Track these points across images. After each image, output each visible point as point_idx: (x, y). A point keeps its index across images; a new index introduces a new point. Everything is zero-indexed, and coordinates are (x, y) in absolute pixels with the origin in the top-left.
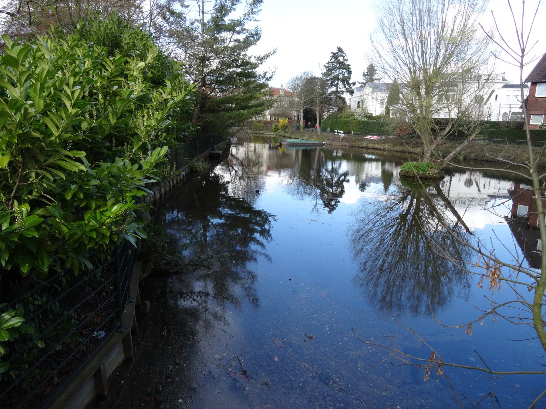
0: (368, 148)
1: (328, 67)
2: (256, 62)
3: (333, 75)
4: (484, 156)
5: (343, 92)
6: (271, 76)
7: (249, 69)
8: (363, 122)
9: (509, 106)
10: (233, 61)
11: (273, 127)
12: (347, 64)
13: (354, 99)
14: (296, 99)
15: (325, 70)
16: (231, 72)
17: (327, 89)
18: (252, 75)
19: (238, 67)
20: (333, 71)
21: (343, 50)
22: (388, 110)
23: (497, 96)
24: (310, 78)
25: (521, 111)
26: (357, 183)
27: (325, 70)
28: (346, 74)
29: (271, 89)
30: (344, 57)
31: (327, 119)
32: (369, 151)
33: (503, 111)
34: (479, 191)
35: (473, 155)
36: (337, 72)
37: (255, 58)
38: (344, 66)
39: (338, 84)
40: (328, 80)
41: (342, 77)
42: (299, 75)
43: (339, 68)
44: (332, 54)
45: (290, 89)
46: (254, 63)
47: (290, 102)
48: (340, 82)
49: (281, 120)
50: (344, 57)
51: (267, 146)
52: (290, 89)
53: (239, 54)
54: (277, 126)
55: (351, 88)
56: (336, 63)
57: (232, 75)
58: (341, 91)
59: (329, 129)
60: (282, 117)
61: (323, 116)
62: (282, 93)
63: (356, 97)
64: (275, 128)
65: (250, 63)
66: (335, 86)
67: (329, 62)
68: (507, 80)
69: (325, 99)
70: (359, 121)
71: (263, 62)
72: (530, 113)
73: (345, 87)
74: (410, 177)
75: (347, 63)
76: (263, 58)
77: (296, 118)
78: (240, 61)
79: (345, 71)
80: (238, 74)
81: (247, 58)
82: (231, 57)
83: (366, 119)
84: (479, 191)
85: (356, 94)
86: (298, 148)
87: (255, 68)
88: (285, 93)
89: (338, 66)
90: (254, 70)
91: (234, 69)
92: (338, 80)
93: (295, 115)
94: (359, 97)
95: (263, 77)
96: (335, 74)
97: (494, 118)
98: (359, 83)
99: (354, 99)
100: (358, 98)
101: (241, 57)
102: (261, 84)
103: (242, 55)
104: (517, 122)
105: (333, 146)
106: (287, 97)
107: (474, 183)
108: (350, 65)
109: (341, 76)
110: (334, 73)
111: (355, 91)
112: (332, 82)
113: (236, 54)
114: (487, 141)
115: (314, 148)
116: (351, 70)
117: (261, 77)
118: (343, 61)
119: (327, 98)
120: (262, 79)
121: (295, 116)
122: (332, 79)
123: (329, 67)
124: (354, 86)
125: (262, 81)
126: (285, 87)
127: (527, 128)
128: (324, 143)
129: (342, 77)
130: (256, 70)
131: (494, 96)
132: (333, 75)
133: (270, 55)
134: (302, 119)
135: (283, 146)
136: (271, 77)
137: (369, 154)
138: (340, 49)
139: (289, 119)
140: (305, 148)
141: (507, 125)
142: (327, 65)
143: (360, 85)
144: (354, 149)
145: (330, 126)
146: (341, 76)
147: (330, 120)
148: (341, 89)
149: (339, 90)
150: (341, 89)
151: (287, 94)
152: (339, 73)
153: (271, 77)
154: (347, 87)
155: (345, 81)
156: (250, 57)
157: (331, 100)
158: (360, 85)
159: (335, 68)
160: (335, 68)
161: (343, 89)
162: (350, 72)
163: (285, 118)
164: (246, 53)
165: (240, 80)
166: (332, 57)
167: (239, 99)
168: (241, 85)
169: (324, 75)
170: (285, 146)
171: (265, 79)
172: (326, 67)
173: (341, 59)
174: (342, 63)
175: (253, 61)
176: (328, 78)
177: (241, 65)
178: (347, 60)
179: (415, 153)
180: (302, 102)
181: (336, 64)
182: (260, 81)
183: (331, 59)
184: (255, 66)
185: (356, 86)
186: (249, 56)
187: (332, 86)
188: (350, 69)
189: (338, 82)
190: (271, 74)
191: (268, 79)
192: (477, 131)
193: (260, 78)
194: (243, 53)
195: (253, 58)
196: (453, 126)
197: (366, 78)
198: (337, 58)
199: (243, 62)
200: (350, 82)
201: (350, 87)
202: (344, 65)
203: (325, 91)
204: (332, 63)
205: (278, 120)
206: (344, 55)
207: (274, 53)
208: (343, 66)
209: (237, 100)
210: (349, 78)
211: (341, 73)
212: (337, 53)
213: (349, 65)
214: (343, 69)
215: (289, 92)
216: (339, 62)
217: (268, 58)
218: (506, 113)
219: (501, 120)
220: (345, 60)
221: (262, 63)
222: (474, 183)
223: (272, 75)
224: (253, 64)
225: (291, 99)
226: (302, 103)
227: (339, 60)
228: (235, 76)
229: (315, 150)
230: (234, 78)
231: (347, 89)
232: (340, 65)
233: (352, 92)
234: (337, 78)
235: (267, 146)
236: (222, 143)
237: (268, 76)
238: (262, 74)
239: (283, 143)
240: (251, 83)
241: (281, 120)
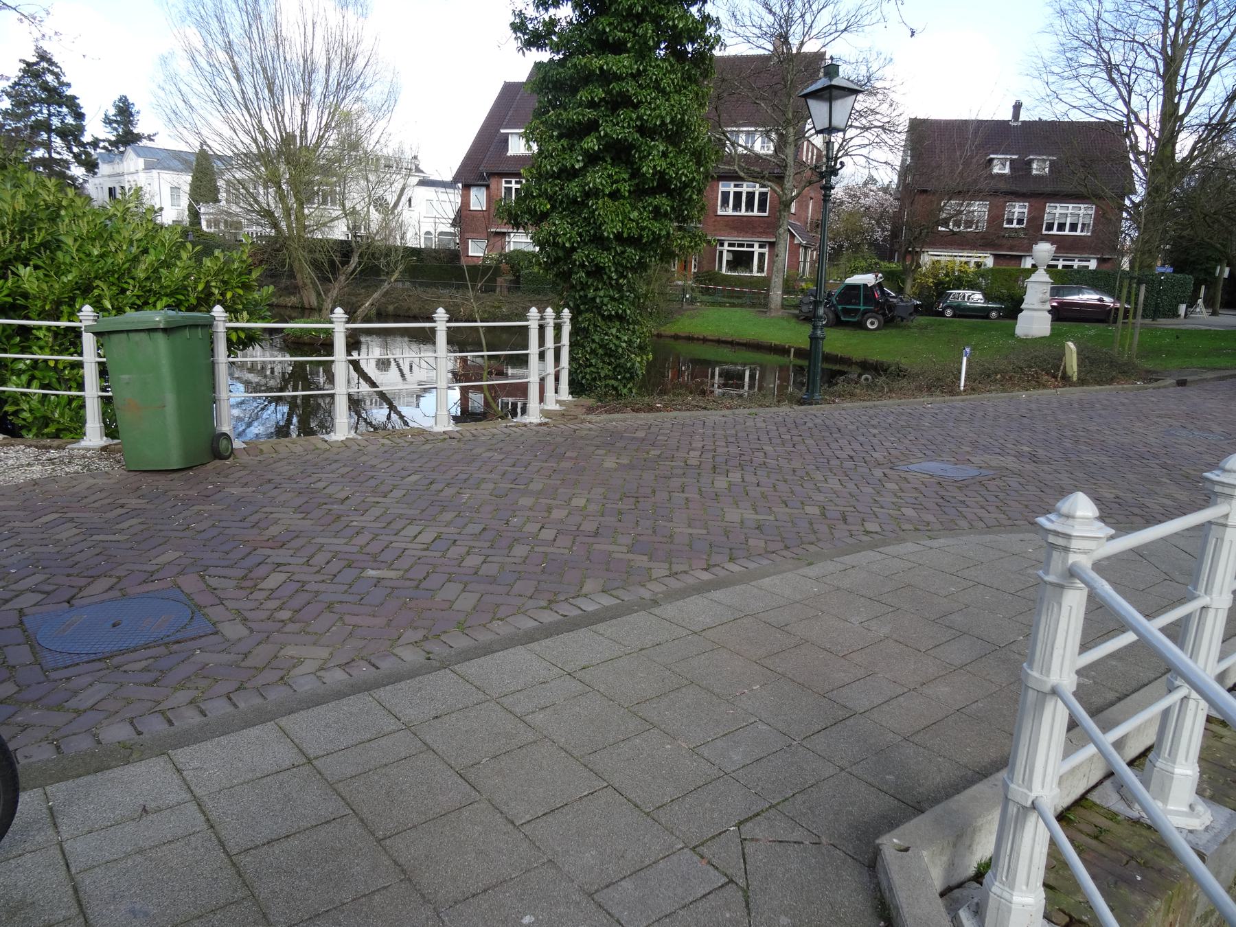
4: (409, 309)
5: (66, 162)
9: (432, 220)
12: (68, 93)
21: (55, 59)
22: (195, 215)
23: (410, 200)
25: (878, 841)
28: (70, 120)
30: (57, 76)
33: (423, 230)
34: (403, 375)
35: (391, 308)
38: (57, 96)
44: (23, 66)
50: (57, 76)
68: (422, 172)
72: (467, 235)
73: (70, 150)
74: (305, 344)
75: (69, 92)
84: (403, 375)
85: (104, 169)
92: (50, 130)
94: (110, 176)
96: (40, 117)
97: (412, 242)
100: (107, 179)
104: (449, 250)
107: (393, 364)
108: (77, 98)
110: (35, 114)
114: (408, 284)
116: (82, 111)
127: (463, 262)
131: (404, 199)
132: (33, 118)
138: (43, 56)
141: (434, 254)
146: (55, 122)
152: (50, 115)
155: (71, 135)
159: (35, 100)
160: (35, 100)
162: (80, 116)
166: (25, 71)
174: (55, 89)
178: (69, 85)
179: (285, 307)
188: (78, 106)
192: (400, 268)
196: (361, 256)
197: (115, 129)
200: (86, 138)
202: (60, 95)
204: (25, 86)
206: (56, 70)
210: (81, 129)
212: (37, 63)
214: (60, 106)
216: (45, 87)
218: (428, 233)
219: (423, 246)
220: (62, 84)
222: (393, 364)
234: (46, 126)
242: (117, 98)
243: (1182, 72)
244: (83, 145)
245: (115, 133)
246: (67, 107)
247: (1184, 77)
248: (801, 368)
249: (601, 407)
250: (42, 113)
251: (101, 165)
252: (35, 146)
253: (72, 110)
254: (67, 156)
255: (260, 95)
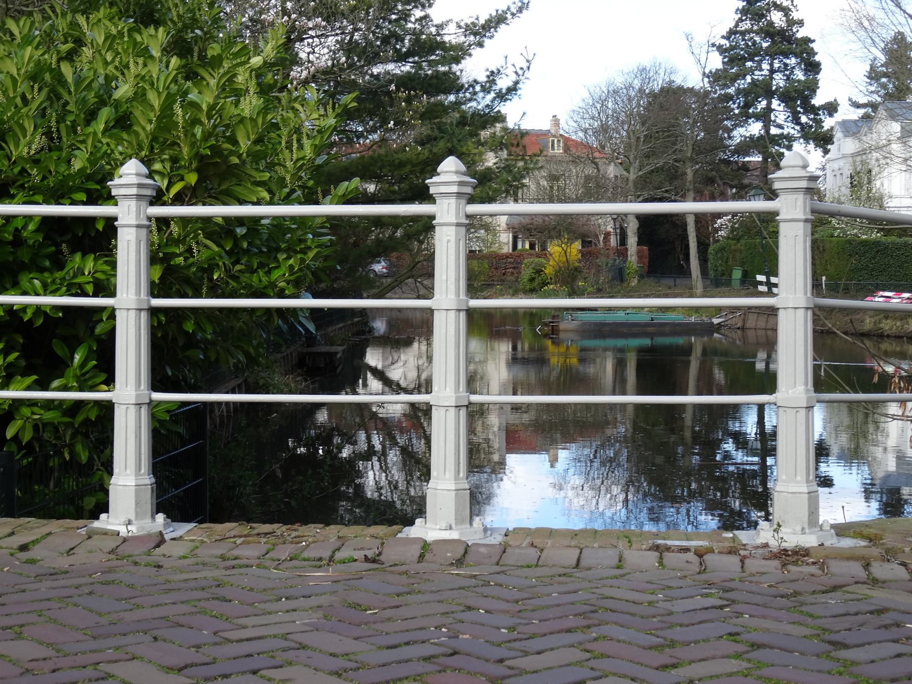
0: (881, 336)
1: (726, 50)
2: (462, 39)
3: (749, 79)
5: (790, 138)
6: (510, 84)
7: (437, 63)
8: (865, 243)
10: (386, 40)
11: (526, 273)
13: (835, 165)
14: (612, 171)
15: (716, 62)
16: (377, 77)
17: (729, 131)
18: (450, 83)
19: (401, 58)
20: (749, 64)
24: (662, 89)
26: (867, 498)
27: (716, 62)
28: (799, 75)
29: (502, 463)
31: (728, 238)
32: (886, 346)
36: (765, 66)
37: (460, 27)
39: (769, 110)
40: (728, 98)
41: (782, 84)
42: (619, 81)
43: (772, 54)
45: (585, 131)
46: (453, 42)
47: (588, 178)
48: (775, 103)
49: (554, 248)
51: (504, 347)
52: (585, 131)
53: (405, 16)
54: (539, 272)
55: (819, 122)
56: (757, 33)
57: (383, 86)
58: (782, 136)
59: (737, 274)
60: (559, 237)
61: (716, 230)
62: (559, 151)
63: (844, 156)
64: (532, 280)
65: (442, 45)
66: (758, 117)
67: (732, 33)
69: (722, 166)
70: (849, 242)
71: (487, 42)
73: (796, 120)
76: (483, 27)
77: (613, 241)
78: (408, 37)
79: (792, 61)
80: (405, 82)
81: (433, 30)
82: (378, 26)
83: (875, 236)
85: (844, 145)
86: (620, 343)
87: (457, 61)
88: (567, 149)
89: (765, 45)
90: (455, 68)
91: (390, 67)
92: (769, 94)
93: (610, 228)
95: (486, 90)
98: (857, 105)
99: (835, 165)
101: (410, 25)
102: (476, 114)
103: (413, 19)
105: (751, 334)
106: (575, 161)
109: (779, 80)
110: (751, 71)
111: (838, 135)
112: (747, 105)
113: (394, 17)
115: (680, 341)
116: (817, 58)
117: (478, 88)
118: (784, 25)
119: (727, 162)
120: (481, 95)
121: (607, 234)
122: (745, 92)
123: (732, 48)
124: (831, 115)
125: (483, 101)
126: (569, 127)
128: (716, 321)
129: (782, 84)
130: (460, 66)
132: (749, 79)
133: (509, 16)
134: (632, 240)
135: (562, 335)
136: (513, 89)
137: (887, 356)
139: (585, 243)
140: (646, 342)
142: (724, 42)
143: (861, 112)
144: (829, 341)
145: (742, 264)
146: (779, 80)
147: (743, 242)
148: (780, 127)
149: (774, 131)
150: (780, 127)
151: (574, 150)
152: (772, 71)
153: (513, 89)
154: (804, 119)
156: (440, 27)
157: (747, 170)
158: (861, 112)
160: (754, 53)
161: (791, 129)
162: (813, 67)
163: (571, 241)
164: (429, 11)
165: (409, 100)
167: (408, 162)
168: (412, 118)
169: (716, 77)
170: (572, 336)
171: (493, 95)
172: (720, 49)
173: (777, 18)
175: (451, 36)
176: (731, 91)
177: (410, 53)
178: (801, 23)
180: (632, 176)
181: (757, 39)
182: (474, 104)
183: (741, 20)
184: (458, 53)
185: (839, 117)
186: (437, 20)
187: (749, 117)
188: (813, 53)
189: (769, 103)
190: (514, 77)
191: (502, 96)
193: (475, 93)
194: (418, 13)
195: (451, 28)
197: (884, 86)
198: (763, 16)
199: (416, 41)
201: (814, 120)
203: (722, 139)
204: (743, 33)
205: (544, 248)
207: (520, 10)
208: (785, 46)
209: (402, 164)
210: (812, 87)
211: (779, 71)
213: (807, 41)
215: (578, 144)
216: (769, 32)
217: (503, 26)
220: (791, 22)
221: (480, 45)
223: (517, 83)
224: (453, 47)
225: (590, 170)
226: (631, 184)
227: (771, 24)
228: (393, 87)
229: (687, 351)
230: (389, 93)
231: (803, 127)
232: (773, 42)
233: (824, 140)
234: (764, 89)
235: (504, 347)
236: (341, 325)
237: (503, 83)
238: (482, 78)
239: (563, 325)
240: (444, 109)
241: (554, 248)
242: (835, 482)
243: (618, 237)
244: (814, 110)
245: (882, 92)
246: (796, 57)
247: (616, 235)
248: (475, 27)
249: (761, 189)
250: (761, 70)
251: (832, 459)
252: (745, 117)
253: (802, 59)
254: (791, 129)
255: (302, 602)
